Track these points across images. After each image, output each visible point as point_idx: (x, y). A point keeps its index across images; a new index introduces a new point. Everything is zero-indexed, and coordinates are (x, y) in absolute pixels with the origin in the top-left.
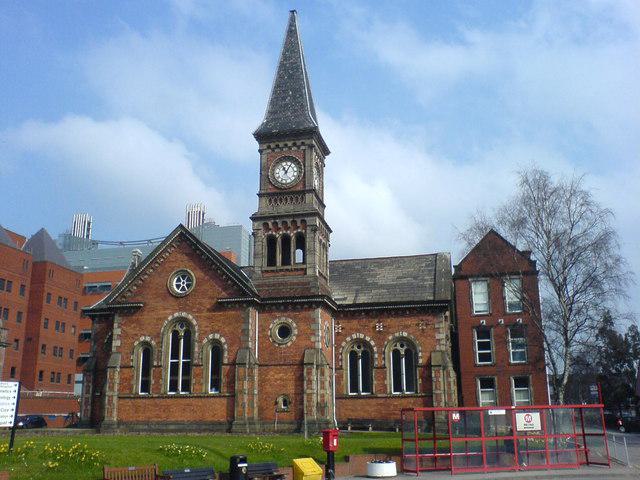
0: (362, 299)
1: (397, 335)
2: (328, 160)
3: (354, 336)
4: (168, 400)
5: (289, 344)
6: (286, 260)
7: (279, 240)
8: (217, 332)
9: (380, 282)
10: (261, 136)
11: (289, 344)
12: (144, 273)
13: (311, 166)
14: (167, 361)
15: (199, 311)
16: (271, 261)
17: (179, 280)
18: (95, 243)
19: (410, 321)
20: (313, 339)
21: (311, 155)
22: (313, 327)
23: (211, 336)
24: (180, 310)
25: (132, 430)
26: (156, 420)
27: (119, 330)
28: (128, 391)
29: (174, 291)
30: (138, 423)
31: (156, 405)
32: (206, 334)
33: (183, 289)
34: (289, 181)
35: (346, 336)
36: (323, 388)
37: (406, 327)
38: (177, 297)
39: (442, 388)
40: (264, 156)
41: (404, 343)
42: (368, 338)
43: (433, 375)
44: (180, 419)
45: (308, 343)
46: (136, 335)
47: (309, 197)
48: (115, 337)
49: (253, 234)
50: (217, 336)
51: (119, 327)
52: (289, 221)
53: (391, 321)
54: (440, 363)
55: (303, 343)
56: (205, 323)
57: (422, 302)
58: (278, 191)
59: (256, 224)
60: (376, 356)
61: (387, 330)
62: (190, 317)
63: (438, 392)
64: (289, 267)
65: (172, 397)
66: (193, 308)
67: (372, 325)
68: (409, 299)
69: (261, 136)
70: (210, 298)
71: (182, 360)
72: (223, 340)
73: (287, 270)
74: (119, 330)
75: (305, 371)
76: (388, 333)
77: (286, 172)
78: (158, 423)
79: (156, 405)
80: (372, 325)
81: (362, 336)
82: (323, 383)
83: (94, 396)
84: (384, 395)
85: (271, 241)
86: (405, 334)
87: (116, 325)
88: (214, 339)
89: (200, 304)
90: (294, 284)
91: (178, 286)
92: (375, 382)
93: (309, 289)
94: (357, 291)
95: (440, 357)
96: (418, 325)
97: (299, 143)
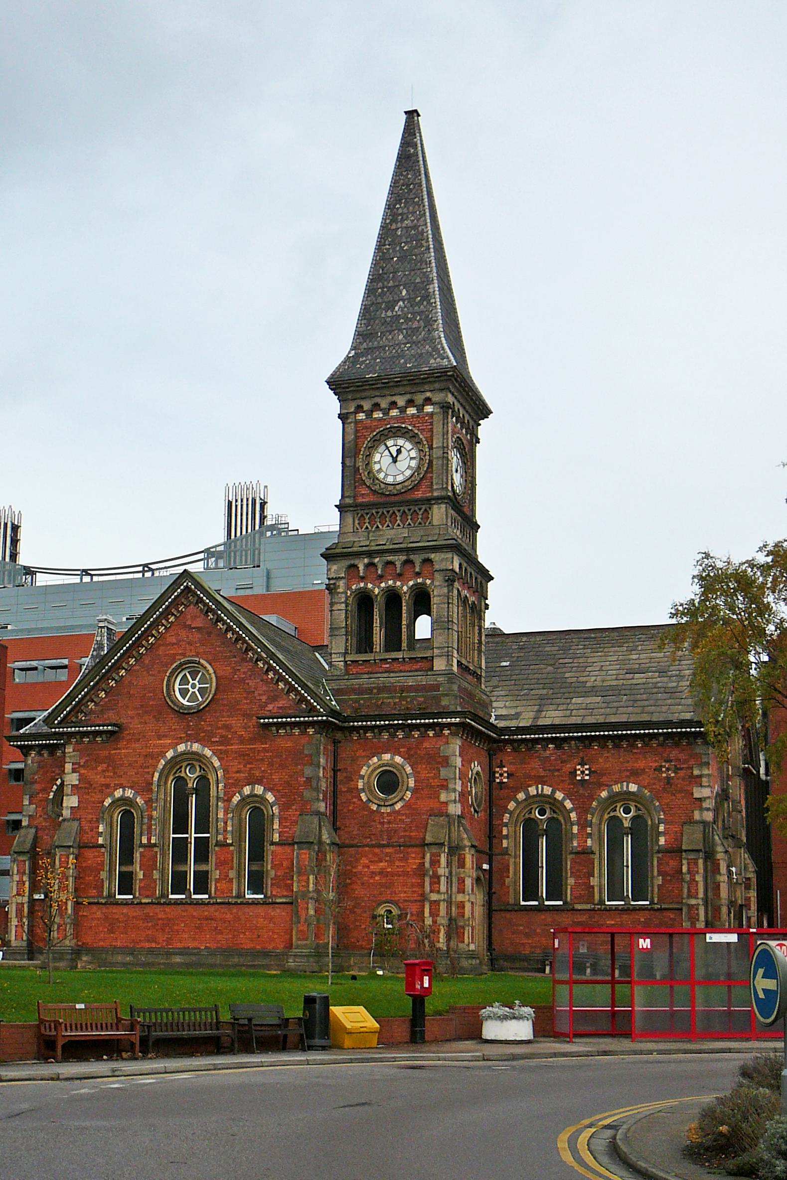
0: (552, 716)
1: (616, 788)
2: (485, 428)
3: (532, 791)
4: (168, 909)
5: (398, 806)
6: (393, 642)
7: (198, 679)
8: (259, 782)
9: (591, 681)
10: (336, 384)
11: (398, 806)
12: (117, 667)
13: (444, 448)
14: (163, 836)
15: (225, 741)
16: (365, 643)
17: (184, 681)
18: (29, 571)
19: (646, 762)
20: (443, 797)
21: (445, 424)
22: (444, 773)
23: (247, 790)
24: (189, 738)
25: (104, 963)
26: (147, 945)
27: (75, 776)
28: (94, 892)
29: (175, 702)
30: (115, 950)
31: (147, 918)
32: (233, 786)
33: (193, 698)
34: (400, 478)
35: (517, 790)
36: (461, 890)
37: (634, 775)
38: (182, 713)
39: (701, 895)
40: (351, 428)
41: (547, 807)
42: (559, 795)
43: (685, 869)
44: (191, 945)
45: (432, 804)
46: (108, 786)
47: (439, 513)
48: (67, 790)
49: (328, 587)
50: (259, 790)
51: (74, 771)
52: (399, 559)
53: (608, 759)
54: (701, 847)
55: (425, 805)
56: (235, 765)
57: (669, 724)
58: (382, 500)
59: (334, 567)
60: (575, 829)
61: (598, 779)
62: (208, 752)
63: (693, 902)
64: (399, 655)
65: (177, 903)
66: (211, 734)
67: (568, 767)
68: (645, 718)
69: (336, 384)
70: (247, 715)
71: (194, 835)
72: (270, 797)
73: (395, 660)
74: (75, 776)
75: (428, 856)
76: (601, 786)
77: (395, 460)
78: (151, 951)
79: (147, 918)
80: (568, 767)
81: (548, 790)
82: (461, 881)
83: (32, 902)
84: (588, 907)
85: (364, 601)
86: (633, 788)
87: (68, 767)
88: (252, 795)
89: (228, 727)
90: (410, 689)
91: (184, 693)
92: (571, 881)
93: (437, 699)
94: (542, 698)
95: (699, 835)
96: (659, 769)
97: (419, 398)
